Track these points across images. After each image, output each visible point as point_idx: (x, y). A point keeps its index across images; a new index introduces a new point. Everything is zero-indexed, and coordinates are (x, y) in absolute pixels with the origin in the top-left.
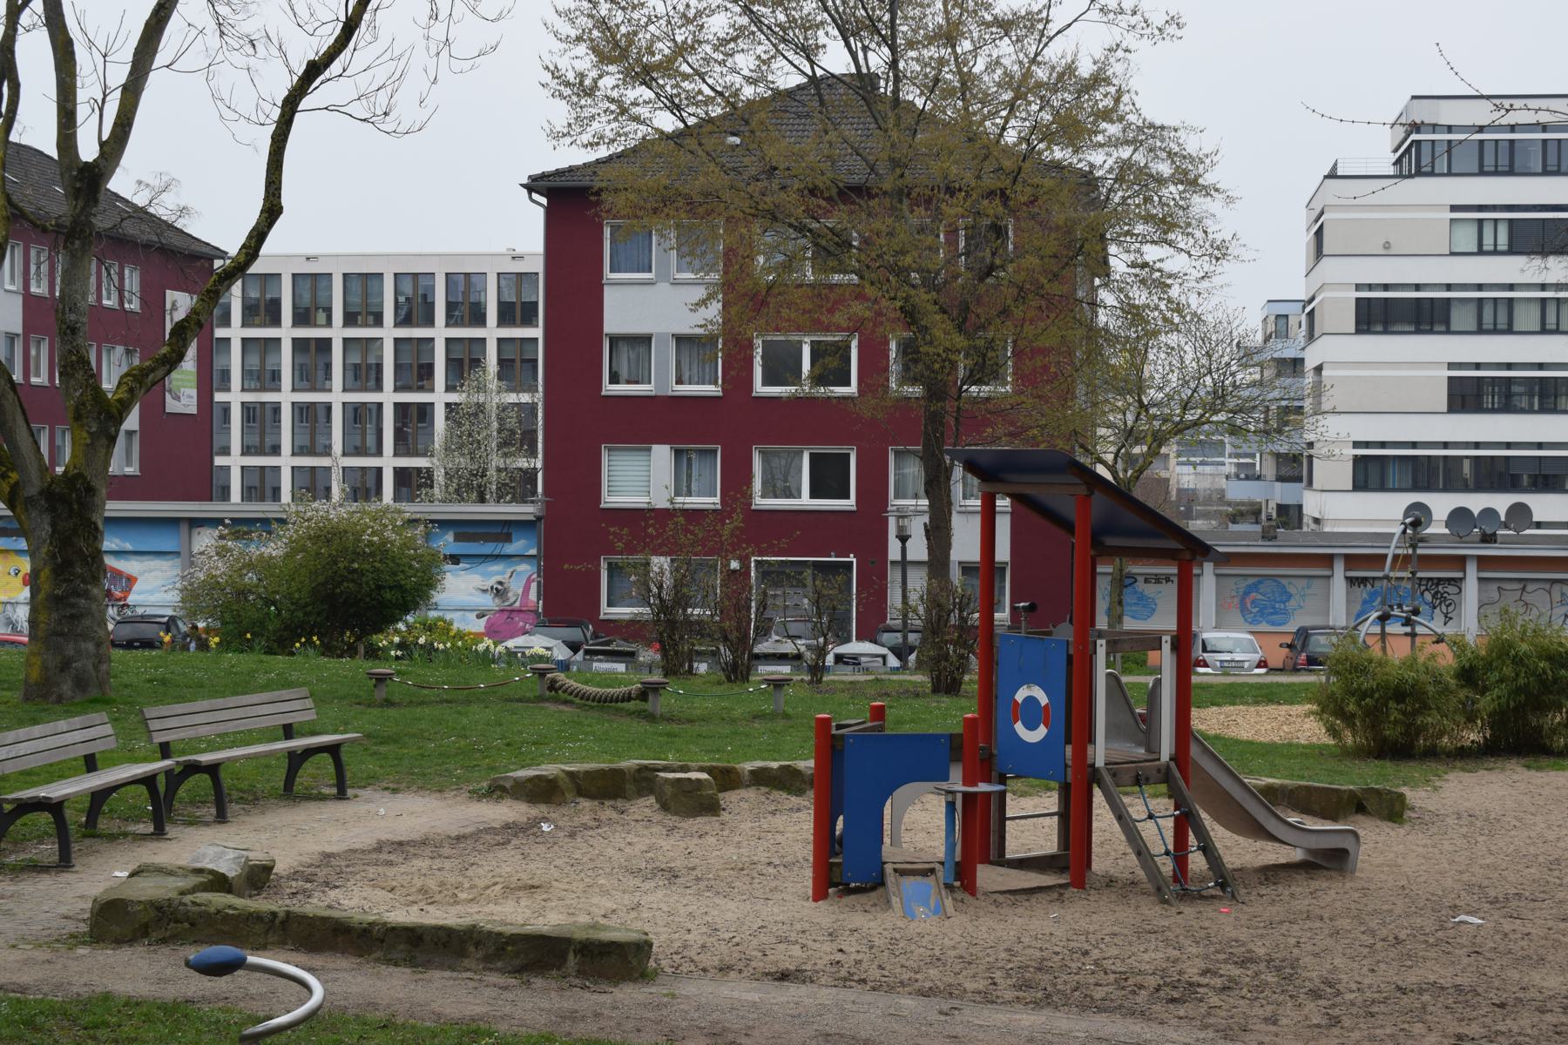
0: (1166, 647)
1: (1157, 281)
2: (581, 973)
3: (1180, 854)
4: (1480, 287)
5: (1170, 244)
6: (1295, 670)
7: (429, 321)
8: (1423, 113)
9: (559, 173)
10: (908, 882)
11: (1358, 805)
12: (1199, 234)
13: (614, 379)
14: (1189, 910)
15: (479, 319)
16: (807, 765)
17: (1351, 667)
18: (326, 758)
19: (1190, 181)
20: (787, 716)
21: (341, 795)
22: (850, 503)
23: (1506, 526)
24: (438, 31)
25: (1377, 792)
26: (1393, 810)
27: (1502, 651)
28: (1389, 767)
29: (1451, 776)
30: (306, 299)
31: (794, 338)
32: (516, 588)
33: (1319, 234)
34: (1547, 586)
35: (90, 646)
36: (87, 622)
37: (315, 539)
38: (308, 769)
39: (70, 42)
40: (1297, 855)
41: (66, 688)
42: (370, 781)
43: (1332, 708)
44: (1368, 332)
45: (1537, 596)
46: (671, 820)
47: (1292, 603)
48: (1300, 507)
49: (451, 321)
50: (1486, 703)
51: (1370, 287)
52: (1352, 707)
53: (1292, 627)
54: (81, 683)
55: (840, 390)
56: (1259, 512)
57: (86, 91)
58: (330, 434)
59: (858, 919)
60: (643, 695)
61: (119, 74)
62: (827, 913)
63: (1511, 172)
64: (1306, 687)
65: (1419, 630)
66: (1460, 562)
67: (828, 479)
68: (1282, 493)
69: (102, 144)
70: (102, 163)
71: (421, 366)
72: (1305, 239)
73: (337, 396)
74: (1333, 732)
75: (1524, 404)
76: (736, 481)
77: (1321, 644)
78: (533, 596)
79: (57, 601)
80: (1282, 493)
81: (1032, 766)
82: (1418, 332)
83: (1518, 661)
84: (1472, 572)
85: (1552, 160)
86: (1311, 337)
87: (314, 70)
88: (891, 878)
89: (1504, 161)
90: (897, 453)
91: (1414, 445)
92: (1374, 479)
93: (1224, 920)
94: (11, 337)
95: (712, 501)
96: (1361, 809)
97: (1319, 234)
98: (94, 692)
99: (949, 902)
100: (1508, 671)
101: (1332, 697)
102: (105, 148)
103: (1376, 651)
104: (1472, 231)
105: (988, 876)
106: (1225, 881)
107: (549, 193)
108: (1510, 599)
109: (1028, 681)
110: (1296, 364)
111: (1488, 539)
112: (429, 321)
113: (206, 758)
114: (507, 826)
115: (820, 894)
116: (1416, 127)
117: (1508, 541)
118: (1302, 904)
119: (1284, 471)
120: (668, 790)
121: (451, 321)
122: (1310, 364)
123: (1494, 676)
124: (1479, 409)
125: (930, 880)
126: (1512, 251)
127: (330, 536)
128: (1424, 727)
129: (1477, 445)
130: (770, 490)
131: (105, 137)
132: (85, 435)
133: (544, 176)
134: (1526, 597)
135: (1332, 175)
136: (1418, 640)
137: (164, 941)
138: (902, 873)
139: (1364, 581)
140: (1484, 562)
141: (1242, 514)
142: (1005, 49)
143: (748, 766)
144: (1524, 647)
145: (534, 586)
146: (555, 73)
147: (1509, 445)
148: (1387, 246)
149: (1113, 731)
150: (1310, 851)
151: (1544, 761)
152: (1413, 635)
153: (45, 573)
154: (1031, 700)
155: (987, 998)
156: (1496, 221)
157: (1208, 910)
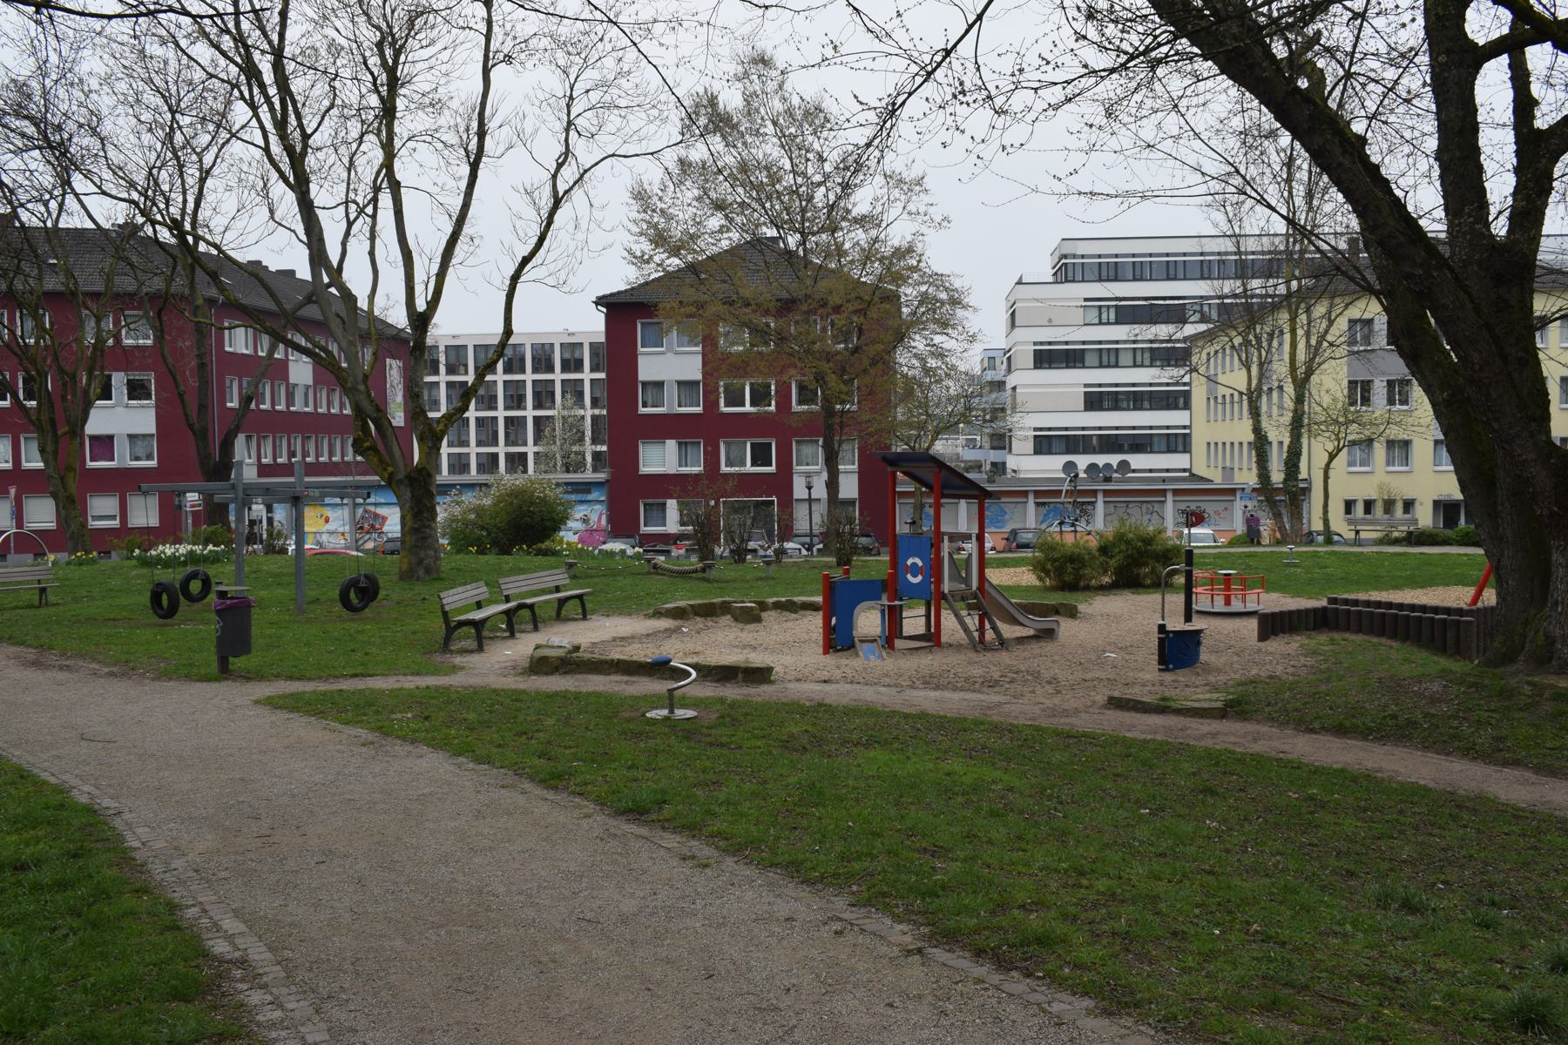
0: (974, 539)
1: (940, 354)
2: (744, 681)
3: (981, 629)
4: (1100, 342)
5: (947, 334)
6: (1010, 551)
8: (1069, 248)
9: (612, 295)
10: (865, 646)
11: (1055, 610)
12: (960, 328)
13: (645, 405)
14: (989, 655)
15: (551, 369)
16: (819, 599)
17: (1048, 548)
18: (577, 601)
19: (955, 302)
20: (773, 579)
21: (585, 618)
22: (772, 469)
23: (1116, 471)
24: (580, 236)
25: (1065, 605)
26: (1072, 613)
27: (1120, 538)
28: (1067, 595)
29: (1097, 598)
30: (453, 360)
31: (742, 381)
32: (594, 518)
33: (1013, 314)
34: (929, 68)
35: (432, 553)
36: (430, 541)
37: (509, 495)
38: (570, 605)
40: (1031, 632)
41: (421, 573)
42: (594, 612)
43: (1040, 567)
44: (1040, 368)
45: (1134, 510)
46: (741, 625)
47: (1007, 517)
48: (1004, 464)
49: (535, 370)
50: (1112, 562)
51: (1042, 343)
52: (1049, 566)
53: (1008, 529)
54: (428, 571)
56: (980, 466)
57: (419, 276)
58: (468, 435)
59: (845, 662)
60: (703, 570)
61: (435, 268)
62: (831, 660)
63: (1116, 280)
64: (1023, 559)
65: (1079, 529)
66: (1094, 493)
67: (761, 456)
68: (995, 456)
69: (427, 303)
72: (1005, 317)
74: (1040, 579)
75: (1125, 405)
76: (712, 460)
77: (1026, 537)
78: (604, 521)
79: (415, 531)
80: (995, 456)
81: (914, 593)
82: (1067, 367)
83: (1128, 542)
84: (1100, 499)
85: (1138, 273)
86: (1009, 370)
87: (526, 261)
88: (858, 644)
89: (1112, 274)
90: (797, 442)
91: (1066, 429)
92: (1045, 447)
93: (1005, 657)
94: (307, 387)
95: (697, 469)
96: (1057, 612)
97: (1013, 314)
98: (435, 575)
99: (884, 654)
100: (1123, 547)
101: (1039, 562)
103: (1058, 538)
104: (1095, 313)
105: (898, 643)
106: (1003, 643)
107: (606, 305)
108: (1121, 511)
109: (914, 555)
110: (999, 385)
111: (1108, 480)
113: (529, 601)
114: (666, 630)
115: (826, 652)
116: (1065, 256)
117: (1118, 481)
118: (1038, 651)
119: (996, 443)
120: (738, 612)
121: (535, 370)
122: (1009, 386)
123: (1117, 550)
124: (1101, 409)
125: (875, 644)
126: (1117, 323)
127: (517, 493)
128: (1084, 575)
129: (1100, 428)
130: (729, 463)
133: (604, 297)
134: (1129, 511)
135: (1019, 283)
136: (1078, 535)
137: (566, 673)
138: (862, 641)
139: (1044, 504)
140: (1106, 493)
141: (971, 467)
142: (860, 235)
143: (771, 600)
144: (1131, 536)
145: (604, 517)
146: (629, 251)
147: (1117, 428)
148: (1050, 320)
149: (951, 578)
150: (1036, 630)
151: (1140, 590)
152: (1075, 531)
153: (409, 517)
154: (914, 564)
155: (913, 687)
156: (1108, 307)
157: (997, 654)
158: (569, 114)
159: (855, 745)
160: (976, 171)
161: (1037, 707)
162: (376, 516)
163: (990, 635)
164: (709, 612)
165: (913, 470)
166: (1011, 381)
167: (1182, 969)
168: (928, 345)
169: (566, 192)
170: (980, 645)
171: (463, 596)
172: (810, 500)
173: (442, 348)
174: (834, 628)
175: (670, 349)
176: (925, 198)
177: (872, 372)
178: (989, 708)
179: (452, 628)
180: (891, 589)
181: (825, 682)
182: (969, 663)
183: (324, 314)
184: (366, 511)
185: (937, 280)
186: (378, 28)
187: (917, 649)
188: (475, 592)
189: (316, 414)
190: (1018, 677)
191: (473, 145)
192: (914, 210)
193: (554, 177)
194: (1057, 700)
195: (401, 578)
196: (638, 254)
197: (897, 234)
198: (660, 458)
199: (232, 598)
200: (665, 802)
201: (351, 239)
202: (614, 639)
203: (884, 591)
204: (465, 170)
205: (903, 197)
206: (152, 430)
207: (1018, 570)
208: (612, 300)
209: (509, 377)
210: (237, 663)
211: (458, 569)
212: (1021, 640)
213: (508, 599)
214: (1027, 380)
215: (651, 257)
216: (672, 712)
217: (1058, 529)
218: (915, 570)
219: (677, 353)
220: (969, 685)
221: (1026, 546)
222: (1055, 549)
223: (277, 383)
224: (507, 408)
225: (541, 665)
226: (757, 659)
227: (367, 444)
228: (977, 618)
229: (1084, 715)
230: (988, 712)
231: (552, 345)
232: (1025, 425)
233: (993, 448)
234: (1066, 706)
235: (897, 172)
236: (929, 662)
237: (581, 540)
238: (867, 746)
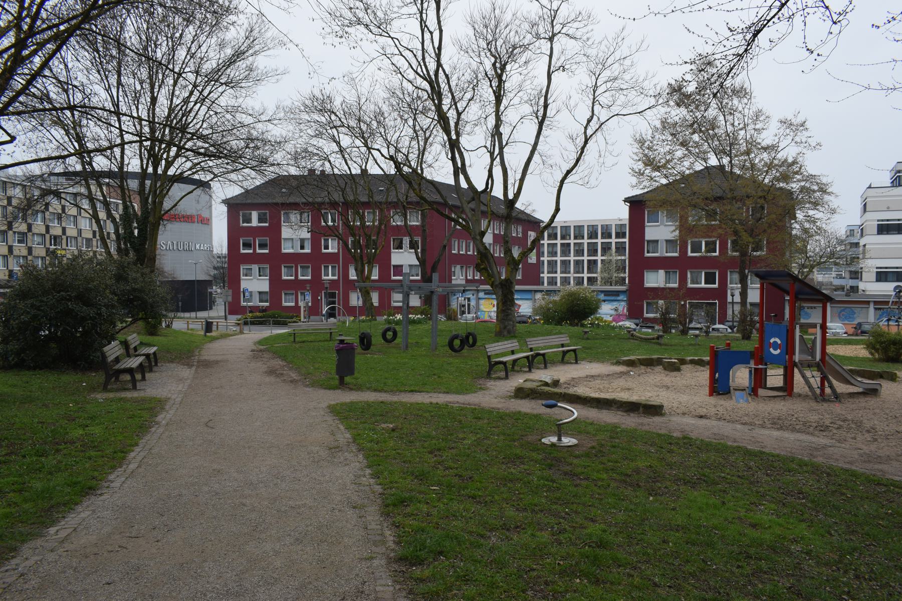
1: (814, 221)
2: (644, 413)
5: (817, 210)
6: (857, 335)
9: (633, 197)
10: (737, 393)
11: (881, 376)
12: (827, 206)
13: (648, 252)
14: (825, 405)
19: (823, 190)
20: (699, 345)
21: (576, 363)
22: (716, 286)
25: (888, 372)
28: (891, 365)
32: (621, 309)
33: (865, 205)
37: (568, 295)
38: (568, 355)
40: (861, 390)
41: (505, 333)
42: (584, 359)
43: (870, 346)
44: (882, 234)
46: (667, 372)
47: (855, 316)
48: (858, 287)
49: (603, 237)
53: (856, 322)
54: (509, 332)
57: (510, 181)
59: (722, 402)
61: (519, 176)
62: (713, 400)
64: (862, 340)
67: (710, 279)
68: (852, 283)
73: (572, 258)
74: (872, 354)
76: (683, 280)
77: (866, 327)
78: (625, 311)
79: (503, 311)
80: (852, 283)
81: (775, 361)
86: (862, 236)
87: (568, 172)
88: (732, 391)
91: (897, 268)
93: (837, 408)
97: (865, 205)
98: (513, 335)
99: (750, 399)
103: (886, 329)
105: (761, 392)
106: (837, 397)
113: (542, 352)
114: (621, 372)
115: (711, 394)
118: (863, 404)
119: (853, 276)
120: (666, 364)
121: (603, 237)
125: (744, 392)
127: (571, 294)
130: (693, 283)
133: (629, 198)
135: (870, 187)
137: (533, 399)
138: (736, 390)
142: (765, 156)
143: (689, 358)
146: (633, 170)
148: (888, 208)
149: (801, 351)
150: (864, 389)
153: (500, 304)
154: (775, 342)
155: (763, 426)
157: (832, 405)
158: (594, 95)
159: (685, 484)
160: (816, 63)
161: (856, 452)
163: (828, 390)
164: (649, 363)
165: (776, 282)
166: (862, 243)
168: (805, 216)
169: (591, 135)
170: (822, 397)
171: (501, 347)
172: (733, 303)
174: (717, 380)
175: (662, 224)
176: (806, 134)
177: (769, 231)
178: (817, 449)
179: (492, 365)
180: (760, 357)
181: (701, 417)
182: (810, 411)
183: (461, 203)
185: (811, 178)
186: (493, 56)
187: (775, 397)
188: (510, 345)
189: (466, 255)
190: (845, 425)
191: (541, 113)
192: (799, 141)
193: (586, 128)
194: (873, 447)
195: (496, 335)
196: (637, 170)
197: (788, 152)
198: (655, 279)
199: (346, 343)
200: (441, 553)
202: (587, 377)
203: (751, 358)
204: (535, 128)
205: (792, 134)
207: (858, 347)
208: (633, 199)
210: (348, 379)
211: (529, 332)
212: (852, 395)
213: (531, 350)
214: (872, 241)
215: (644, 173)
216: (560, 439)
217: (886, 323)
218: (775, 346)
219: (666, 226)
220: (805, 428)
221: (863, 332)
222: (882, 336)
223: (461, 240)
225: (521, 393)
226: (656, 401)
227: (482, 267)
228: (818, 379)
229: (894, 463)
230: (815, 453)
232: (870, 265)
233: (851, 278)
234: (880, 453)
235: (789, 119)
236: (781, 407)
237: (614, 320)
238: (694, 486)
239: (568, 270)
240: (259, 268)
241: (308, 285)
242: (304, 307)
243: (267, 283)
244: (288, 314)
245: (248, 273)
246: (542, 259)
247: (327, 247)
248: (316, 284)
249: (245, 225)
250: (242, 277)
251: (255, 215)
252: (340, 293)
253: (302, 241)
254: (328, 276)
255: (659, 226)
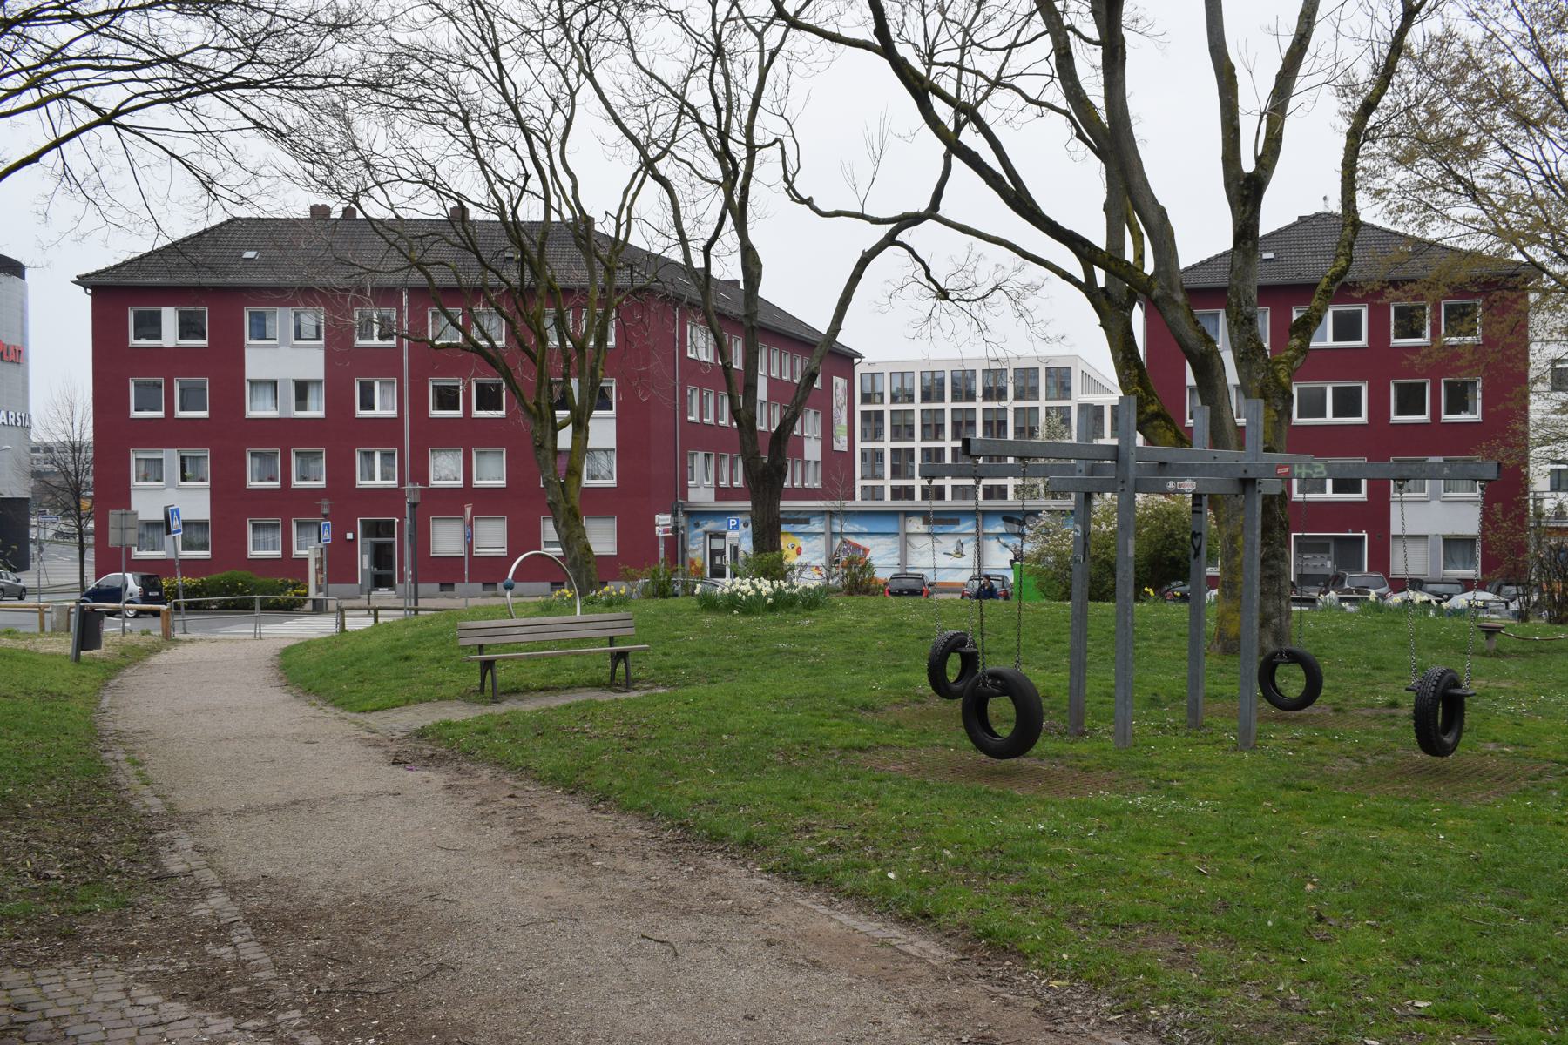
7: (941, 399)
9: (98, 273)
39: (1232, 68)
49: (955, 399)
55: (1464, 417)
58: (883, 466)
70: (1261, 171)
71: (999, 422)
73: (887, 444)
102: (1263, 161)
112: (941, 399)
121: (955, 399)
131: (1259, 153)
132: (1272, 413)
162: (857, 547)
167: (1155, 978)
173: (1010, 374)
184: (844, 542)
189: (715, 427)
201: (709, 236)
206: (613, 445)
209: (927, 406)
224: (923, 438)
231: (974, 372)
239: (878, 470)
240: (183, 459)
241: (325, 502)
242: (318, 560)
243: (205, 498)
244: (270, 580)
245: (154, 470)
246: (959, 444)
247: (368, 404)
248: (342, 493)
249: (144, 343)
250: (134, 483)
251: (169, 318)
252: (404, 524)
253: (302, 388)
254: (372, 478)
255: (276, 347)
